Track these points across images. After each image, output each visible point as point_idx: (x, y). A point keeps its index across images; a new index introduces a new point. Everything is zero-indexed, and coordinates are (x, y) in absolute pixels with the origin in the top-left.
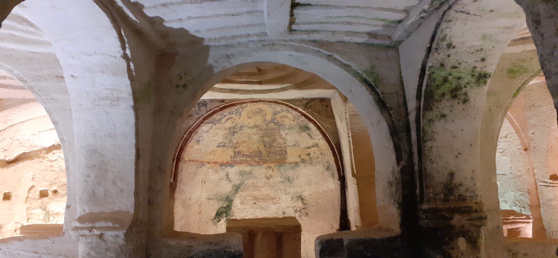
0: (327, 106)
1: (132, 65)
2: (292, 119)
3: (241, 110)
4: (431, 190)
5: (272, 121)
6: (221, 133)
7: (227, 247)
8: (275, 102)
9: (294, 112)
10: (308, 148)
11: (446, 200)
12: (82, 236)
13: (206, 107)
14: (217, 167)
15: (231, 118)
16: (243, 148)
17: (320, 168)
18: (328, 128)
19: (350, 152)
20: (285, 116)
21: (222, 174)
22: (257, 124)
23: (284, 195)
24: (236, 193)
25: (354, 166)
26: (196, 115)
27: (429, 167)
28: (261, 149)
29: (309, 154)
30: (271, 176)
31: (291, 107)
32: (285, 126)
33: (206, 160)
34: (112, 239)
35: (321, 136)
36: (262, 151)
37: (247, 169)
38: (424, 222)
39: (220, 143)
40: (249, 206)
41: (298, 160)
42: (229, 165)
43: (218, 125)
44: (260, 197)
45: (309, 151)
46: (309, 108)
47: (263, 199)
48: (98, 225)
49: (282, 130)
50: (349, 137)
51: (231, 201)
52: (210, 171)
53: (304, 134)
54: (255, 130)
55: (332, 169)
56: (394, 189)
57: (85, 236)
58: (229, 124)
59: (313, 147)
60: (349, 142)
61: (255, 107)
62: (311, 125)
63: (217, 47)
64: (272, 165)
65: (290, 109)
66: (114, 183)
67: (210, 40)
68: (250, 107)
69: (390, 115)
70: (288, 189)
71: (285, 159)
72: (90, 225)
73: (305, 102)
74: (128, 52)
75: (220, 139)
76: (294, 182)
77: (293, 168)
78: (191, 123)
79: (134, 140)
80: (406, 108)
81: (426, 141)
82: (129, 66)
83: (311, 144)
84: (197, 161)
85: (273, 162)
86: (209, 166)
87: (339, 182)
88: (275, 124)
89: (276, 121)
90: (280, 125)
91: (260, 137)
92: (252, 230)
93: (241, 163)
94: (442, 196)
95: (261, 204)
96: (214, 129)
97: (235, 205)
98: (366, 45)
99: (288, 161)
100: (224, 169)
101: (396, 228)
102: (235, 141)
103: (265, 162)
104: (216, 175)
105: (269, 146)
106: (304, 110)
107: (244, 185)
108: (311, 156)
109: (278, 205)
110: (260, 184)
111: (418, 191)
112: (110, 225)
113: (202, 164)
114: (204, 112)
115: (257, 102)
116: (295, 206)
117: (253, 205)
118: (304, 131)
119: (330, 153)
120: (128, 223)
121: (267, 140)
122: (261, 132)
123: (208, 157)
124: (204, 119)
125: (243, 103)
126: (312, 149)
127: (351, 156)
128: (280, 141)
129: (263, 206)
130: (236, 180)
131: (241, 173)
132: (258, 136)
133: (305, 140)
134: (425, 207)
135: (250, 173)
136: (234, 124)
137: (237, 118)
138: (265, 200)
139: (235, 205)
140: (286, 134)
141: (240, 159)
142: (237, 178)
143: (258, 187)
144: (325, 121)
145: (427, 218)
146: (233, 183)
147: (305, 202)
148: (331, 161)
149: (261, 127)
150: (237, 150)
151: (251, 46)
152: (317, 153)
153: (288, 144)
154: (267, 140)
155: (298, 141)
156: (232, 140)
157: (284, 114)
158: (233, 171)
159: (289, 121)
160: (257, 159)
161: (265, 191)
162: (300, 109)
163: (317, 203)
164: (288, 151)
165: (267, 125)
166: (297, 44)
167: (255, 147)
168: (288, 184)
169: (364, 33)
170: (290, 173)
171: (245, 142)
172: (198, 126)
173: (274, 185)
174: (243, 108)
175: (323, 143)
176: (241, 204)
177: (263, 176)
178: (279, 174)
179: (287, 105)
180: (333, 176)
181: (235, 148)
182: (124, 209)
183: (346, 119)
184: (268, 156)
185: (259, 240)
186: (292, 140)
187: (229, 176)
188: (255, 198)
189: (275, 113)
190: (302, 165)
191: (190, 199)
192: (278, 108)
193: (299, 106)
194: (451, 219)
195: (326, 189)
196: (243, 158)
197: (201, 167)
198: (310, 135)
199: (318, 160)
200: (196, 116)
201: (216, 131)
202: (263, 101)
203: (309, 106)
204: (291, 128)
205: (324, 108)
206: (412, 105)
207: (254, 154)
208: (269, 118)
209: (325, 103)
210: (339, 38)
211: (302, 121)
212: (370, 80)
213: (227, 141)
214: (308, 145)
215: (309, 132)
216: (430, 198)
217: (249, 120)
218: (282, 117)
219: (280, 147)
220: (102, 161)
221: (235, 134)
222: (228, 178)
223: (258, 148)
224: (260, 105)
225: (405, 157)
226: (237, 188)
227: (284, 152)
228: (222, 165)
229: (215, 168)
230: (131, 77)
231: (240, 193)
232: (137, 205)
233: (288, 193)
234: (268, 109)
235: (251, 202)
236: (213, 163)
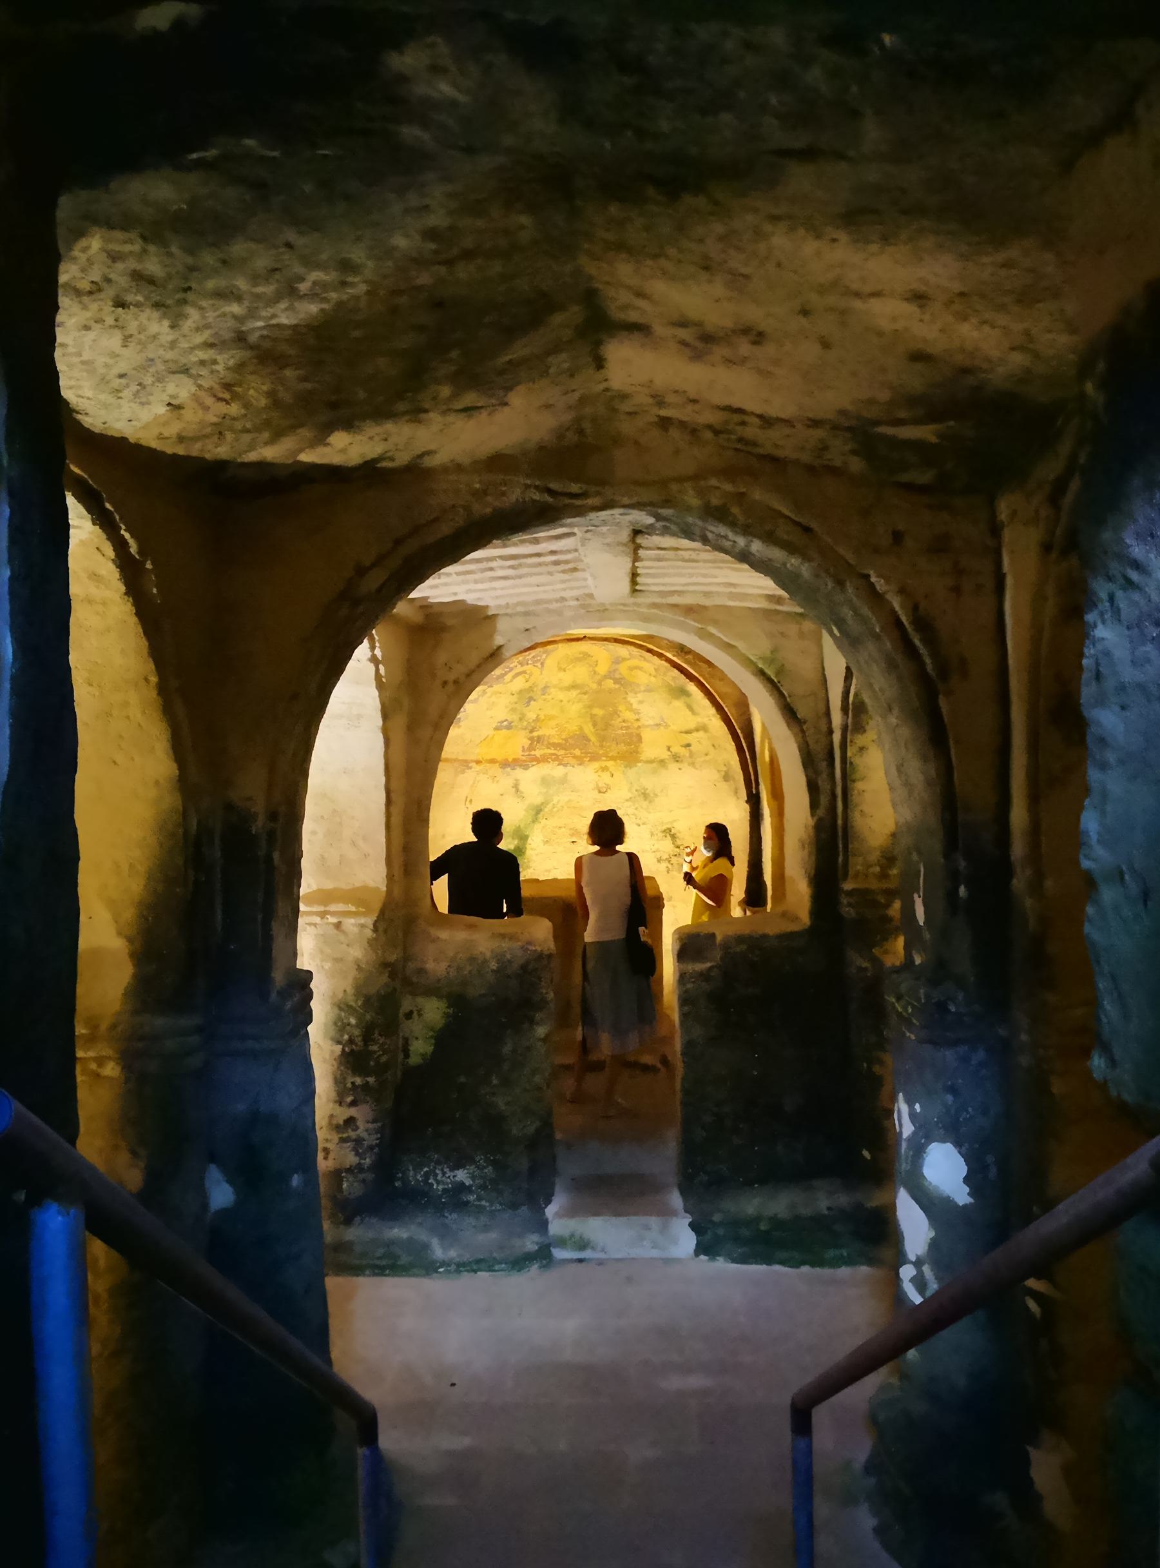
1: (382, 668)
2: (653, 673)
4: (860, 860)
5: (610, 675)
7: (529, 943)
11: (884, 876)
12: (310, 924)
14: (495, 769)
15: (525, 672)
16: (548, 731)
17: (711, 775)
22: (579, 682)
27: (857, 820)
29: (689, 745)
30: (608, 788)
31: (649, 651)
32: (638, 685)
33: (474, 757)
34: (356, 930)
35: (713, 711)
37: (558, 771)
38: (847, 911)
41: (665, 755)
42: (520, 766)
43: (496, 687)
45: (689, 738)
48: (333, 908)
53: (679, 704)
54: (574, 693)
55: (734, 779)
56: (806, 851)
57: (315, 925)
58: (519, 684)
59: (697, 730)
62: (692, 688)
63: (507, 615)
64: (610, 764)
66: (354, 844)
67: (499, 606)
68: (563, 650)
69: (803, 731)
71: (637, 752)
72: (322, 909)
74: (378, 652)
75: (501, 712)
79: (384, 779)
80: (830, 722)
81: (854, 781)
82: (377, 670)
83: (692, 725)
84: (455, 760)
85: (613, 758)
87: (747, 807)
88: (617, 681)
89: (617, 676)
94: (878, 869)
97: (533, 845)
98: (767, 613)
99: (643, 757)
101: (805, 917)
102: (531, 716)
103: (594, 758)
105: (603, 726)
107: (550, 806)
111: (840, 859)
112: (353, 909)
115: (578, 640)
118: (677, 698)
119: (731, 746)
120: (377, 906)
121: (599, 712)
126: (695, 734)
128: (628, 715)
131: (545, 781)
132: (580, 705)
134: (848, 886)
135: (564, 780)
136: (528, 685)
139: (533, 845)
140: (641, 702)
141: (542, 752)
145: (850, 905)
147: (679, 842)
148: (732, 763)
149: (587, 689)
150: (535, 734)
151: (569, 613)
153: (643, 722)
154: (599, 712)
157: (634, 662)
160: (577, 752)
162: (669, 655)
164: (646, 735)
165: (599, 683)
166: (645, 610)
167: (573, 727)
168: (645, 804)
169: (760, 596)
170: (649, 782)
174: (548, 653)
179: (640, 647)
180: (736, 792)
181: (531, 732)
182: (372, 884)
184: (602, 746)
187: (521, 788)
190: (673, 766)
191: (444, 836)
192: (623, 651)
194: (888, 905)
196: (549, 751)
197: (463, 772)
198: (690, 708)
199: (707, 758)
204: (649, 690)
206: (837, 718)
208: (602, 669)
210: (719, 601)
211: (674, 678)
212: (771, 673)
215: (687, 699)
216: (858, 872)
217: (561, 675)
218: (631, 669)
219: (628, 728)
220: (334, 811)
222: (517, 791)
223: (581, 729)
224: (584, 646)
225: (824, 800)
227: (635, 739)
230: (380, 685)
232: (390, 877)
234: (602, 654)
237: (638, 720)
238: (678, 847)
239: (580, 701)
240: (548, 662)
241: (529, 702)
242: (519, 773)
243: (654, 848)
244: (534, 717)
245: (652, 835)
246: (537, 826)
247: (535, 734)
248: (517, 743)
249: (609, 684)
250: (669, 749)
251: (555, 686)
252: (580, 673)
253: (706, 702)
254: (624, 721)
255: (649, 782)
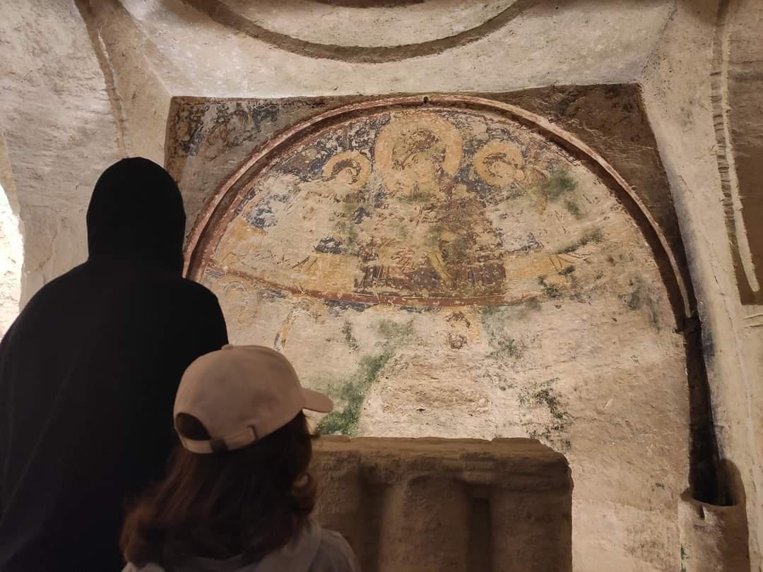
0: (628, 107)
2: (520, 160)
3: (372, 135)
6: (327, 209)
8: (469, 105)
9: (526, 135)
10: (567, 251)
13: (274, 119)
16: (384, 261)
18: (633, 171)
19: (731, 223)
20: (498, 157)
21: (334, 325)
22: (423, 188)
23: (499, 392)
24: (370, 380)
25: (749, 267)
26: (247, 143)
28: (435, 265)
30: (463, 341)
32: (500, 189)
33: (287, 283)
36: (439, 270)
39: (326, 242)
40: (405, 418)
41: (537, 291)
42: (353, 305)
43: (312, 185)
44: (435, 394)
46: (573, 116)
47: (443, 401)
49: (490, 207)
50: (723, 169)
51: (357, 400)
52: (299, 313)
53: (556, 207)
54: (416, 207)
55: (650, 302)
58: (343, 184)
59: (584, 243)
60: (726, 188)
61: (413, 127)
62: (580, 172)
64: (465, 309)
65: (512, 126)
68: (400, 126)
70: (509, 374)
71: (499, 291)
73: (559, 97)
76: (526, 354)
77: (522, 316)
78: (234, 161)
83: (575, 237)
85: (469, 302)
86: (295, 299)
87: (680, 339)
88: (472, 186)
90: (483, 190)
91: (433, 230)
92: (373, 469)
93: (383, 300)
95: (438, 412)
96: (303, 194)
97: (369, 411)
99: (507, 297)
100: (337, 314)
102: (364, 237)
103: (447, 302)
104: (318, 326)
105: (456, 255)
106: (557, 120)
107: (391, 361)
108: (576, 273)
109: (484, 417)
110: (437, 362)
113: (276, 291)
114: (270, 135)
115: (415, 105)
116: (530, 423)
117: (414, 413)
119: (642, 252)
121: (449, 237)
122: (433, 214)
123: (294, 275)
124: (270, 156)
125: (377, 109)
126: (580, 250)
127: (733, 237)
128: (485, 239)
129: (442, 419)
130: (371, 344)
131: (384, 329)
133: (558, 226)
135: (408, 329)
136: (357, 186)
137: (365, 164)
138: (448, 403)
139: (369, 411)
140: (503, 217)
141: (380, 289)
142: (373, 340)
143: (431, 367)
144: (623, 151)
146: (362, 354)
147: (560, 410)
149: (433, 200)
150: (371, 264)
152: (595, 260)
154: (449, 237)
155: (535, 233)
156: (356, 235)
157: (495, 146)
158: (364, 321)
159: (510, 170)
160: (425, 293)
161: (448, 379)
162: (543, 122)
163: (600, 413)
164: (511, 266)
165: (449, 191)
167: (418, 259)
168: (511, 361)
170: (515, 330)
171: (389, 243)
172: (254, 173)
173: (471, 364)
175: (618, 224)
176: (385, 409)
177: (442, 339)
178: (484, 333)
181: (366, 260)
183: (716, 99)
184: (454, 286)
185: (398, 499)
186: (519, 233)
188: (423, 397)
189: (471, 148)
190: (548, 305)
192: (478, 125)
193: (542, 111)
195: (627, 365)
196: (389, 289)
197: (272, 299)
198: (573, 208)
199: (603, 280)
200: (249, 145)
201: (311, 203)
202: (434, 104)
203: (570, 110)
205: (619, 113)
207: (416, 278)
208: (452, 165)
209: (624, 99)
211: (550, 162)
213: (345, 236)
214: (566, 242)
215: (568, 196)
217: (399, 175)
221: (365, 218)
222: (349, 338)
223: (428, 261)
226: (374, 367)
228: (332, 301)
229: (313, 308)
231: (383, 380)
233: (511, 387)
234: (447, 132)
235: (412, 407)
236: (307, 292)
237: (499, 245)
238: (560, 416)
239: (425, 220)
240: (380, 146)
241: (360, 216)
242: (350, 314)
243: (525, 420)
244: (368, 240)
245: (522, 401)
246: (374, 386)
247: (371, 264)
248: (346, 275)
249: (462, 191)
250: (541, 280)
251: (392, 195)
252: (421, 172)
253: (602, 189)
254: (481, 249)
255: (515, 330)
